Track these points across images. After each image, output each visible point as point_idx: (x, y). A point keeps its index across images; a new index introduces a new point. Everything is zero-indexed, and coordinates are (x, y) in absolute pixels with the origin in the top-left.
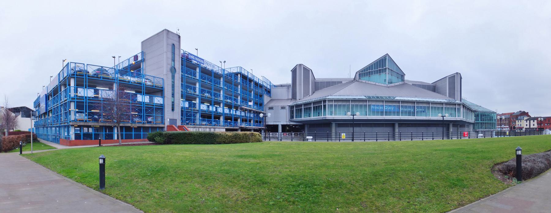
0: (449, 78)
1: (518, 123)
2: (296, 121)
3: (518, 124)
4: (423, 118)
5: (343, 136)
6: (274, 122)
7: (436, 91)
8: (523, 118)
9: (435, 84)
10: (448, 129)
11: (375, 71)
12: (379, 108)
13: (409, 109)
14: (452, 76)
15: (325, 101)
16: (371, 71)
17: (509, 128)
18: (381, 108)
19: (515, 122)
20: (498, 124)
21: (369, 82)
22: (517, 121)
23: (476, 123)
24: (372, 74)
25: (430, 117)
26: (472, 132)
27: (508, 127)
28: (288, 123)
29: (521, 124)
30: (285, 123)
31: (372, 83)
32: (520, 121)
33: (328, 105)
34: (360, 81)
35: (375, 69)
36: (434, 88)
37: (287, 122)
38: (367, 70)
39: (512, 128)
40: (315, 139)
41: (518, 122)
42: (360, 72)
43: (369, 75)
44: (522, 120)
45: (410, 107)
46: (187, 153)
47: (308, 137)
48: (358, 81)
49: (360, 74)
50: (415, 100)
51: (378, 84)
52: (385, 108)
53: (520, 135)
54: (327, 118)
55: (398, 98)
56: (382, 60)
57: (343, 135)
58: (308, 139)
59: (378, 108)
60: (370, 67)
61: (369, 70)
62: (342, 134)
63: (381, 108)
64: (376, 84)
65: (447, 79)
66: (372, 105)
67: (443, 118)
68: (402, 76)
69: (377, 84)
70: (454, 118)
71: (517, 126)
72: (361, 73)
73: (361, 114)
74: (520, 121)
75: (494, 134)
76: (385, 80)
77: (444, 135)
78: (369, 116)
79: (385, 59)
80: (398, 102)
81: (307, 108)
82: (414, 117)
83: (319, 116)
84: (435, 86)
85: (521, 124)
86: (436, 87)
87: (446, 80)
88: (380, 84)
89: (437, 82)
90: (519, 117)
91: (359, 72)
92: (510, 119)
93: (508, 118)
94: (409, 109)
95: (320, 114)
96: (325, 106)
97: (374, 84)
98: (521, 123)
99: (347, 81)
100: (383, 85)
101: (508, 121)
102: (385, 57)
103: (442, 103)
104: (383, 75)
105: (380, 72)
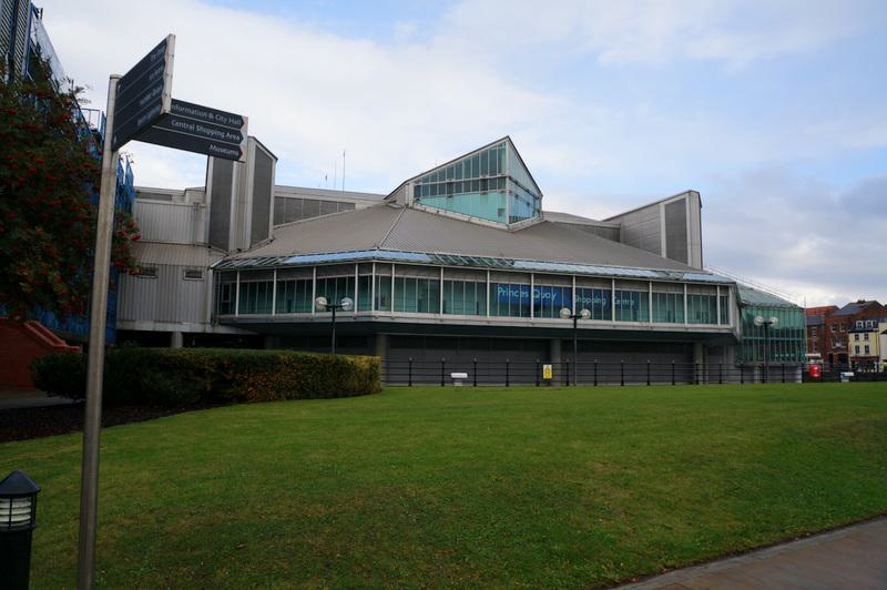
0: (666, 206)
1: (857, 343)
2: (239, 322)
3: (857, 348)
4: (100, 301)
5: (547, 371)
6: (155, 322)
7: (622, 238)
8: (876, 326)
9: (617, 222)
10: (691, 358)
11: (467, 183)
12: (518, 294)
13: (597, 301)
14: (670, 201)
15: (365, 265)
16: (457, 183)
17: (822, 361)
18: (523, 294)
19: (846, 341)
20: (810, 343)
21: (449, 214)
22: (852, 337)
23: (745, 341)
24: (459, 191)
25: (651, 324)
26: (734, 372)
27: (819, 355)
28: (209, 329)
29: (867, 348)
30: (197, 328)
31: (458, 216)
32: (862, 336)
33: (377, 277)
34: (418, 207)
35: (467, 175)
36: (615, 233)
37: (204, 323)
38: (442, 178)
39: (835, 358)
40: (474, 380)
41: (857, 338)
42: (419, 181)
43: (450, 192)
44: (870, 334)
45: (598, 293)
46: (304, 413)
47: (454, 375)
48: (411, 208)
49: (417, 189)
50: (530, 267)
51: (478, 222)
52: (535, 293)
53: (783, 381)
54: (374, 320)
55: (519, 265)
56: (493, 152)
57: (548, 369)
58: (454, 380)
59: (514, 294)
60: (453, 169)
61: (450, 176)
62: (545, 366)
63: (523, 294)
64: (473, 221)
65: (662, 206)
66: (501, 285)
67: (575, 324)
68: (538, 197)
69: (474, 220)
70: (712, 326)
71: (853, 353)
72: (421, 184)
73: (698, 318)
74: (862, 336)
75: (800, 377)
76: (501, 212)
77: (676, 373)
78: (494, 318)
79: (502, 151)
80: (526, 274)
81: (293, 282)
82: (483, 318)
83: (289, 311)
84: (618, 229)
85: (867, 348)
86: (621, 232)
87: (658, 212)
88: (485, 223)
89: (625, 217)
90: (860, 323)
91: (416, 182)
92: (827, 328)
93: (819, 326)
94: (597, 301)
95: (481, 307)
96: (365, 283)
97: (466, 219)
98: (867, 343)
99: (371, 204)
100: (494, 225)
101: (818, 334)
102: (501, 145)
103: (644, 282)
104: (493, 195)
105: (484, 186)
